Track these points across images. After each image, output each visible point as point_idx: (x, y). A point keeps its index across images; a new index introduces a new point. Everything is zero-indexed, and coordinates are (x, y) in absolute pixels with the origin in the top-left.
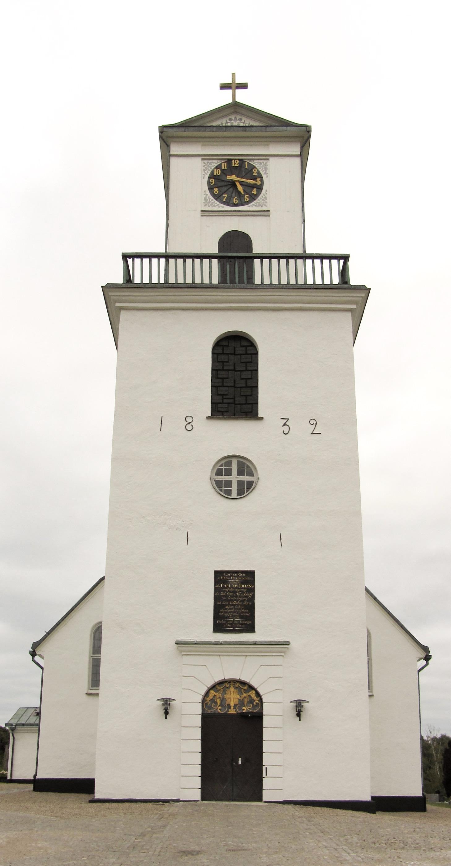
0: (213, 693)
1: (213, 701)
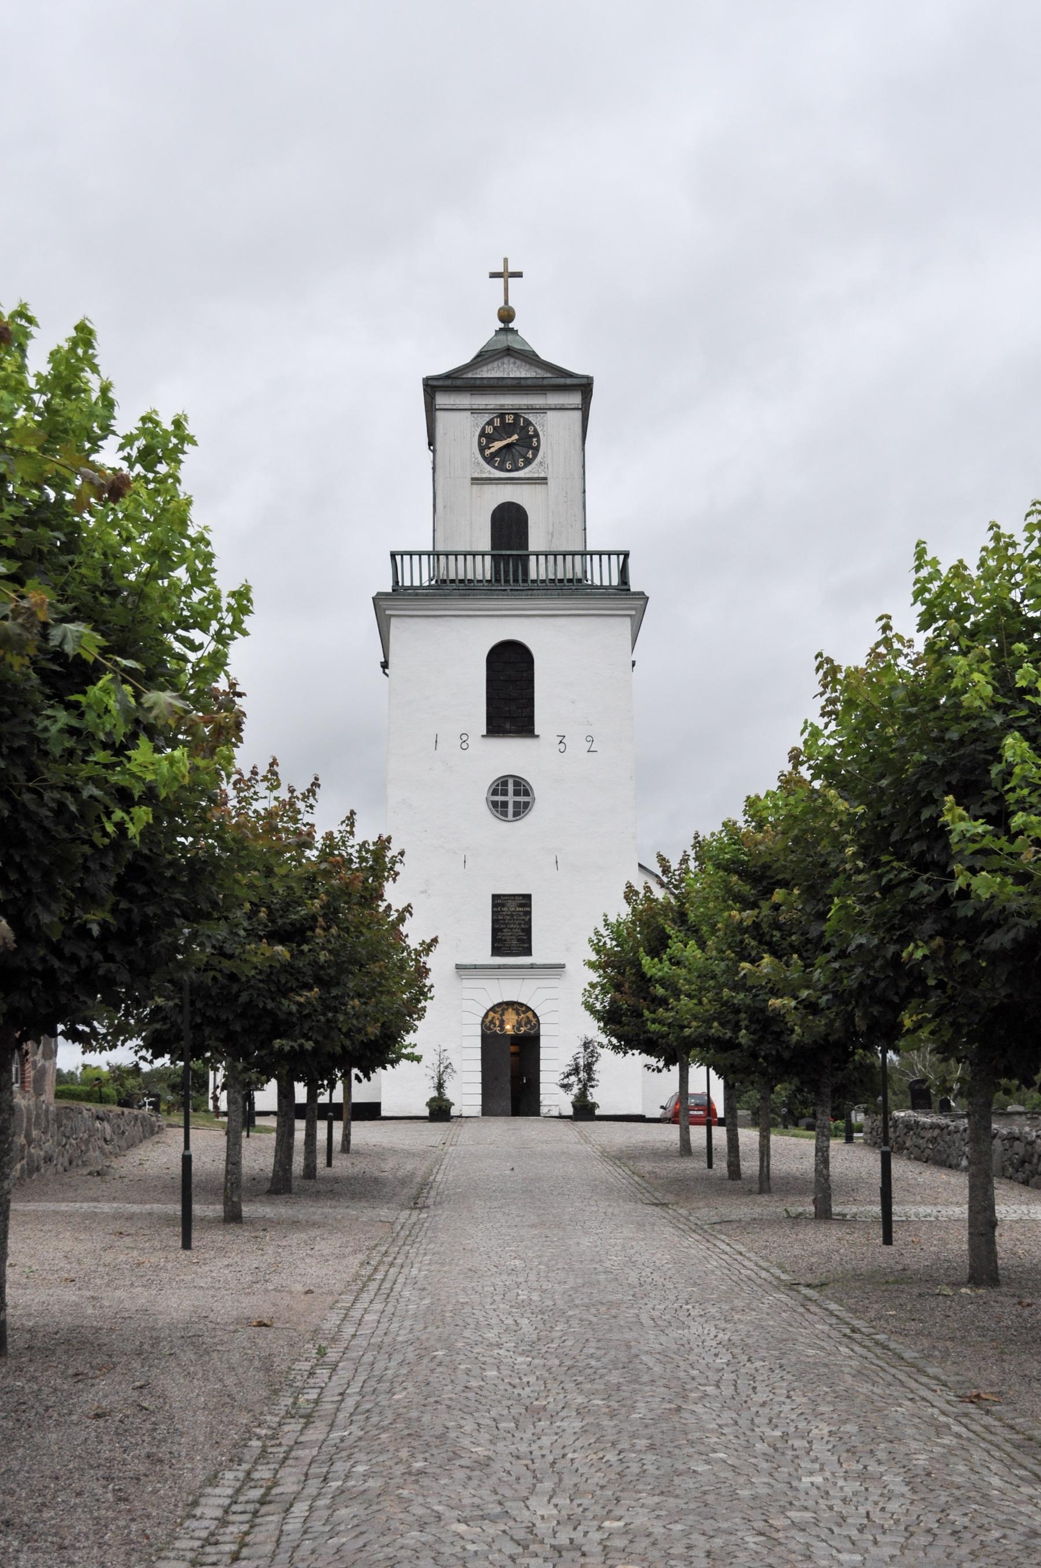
0: (491, 1014)
1: (492, 1022)
